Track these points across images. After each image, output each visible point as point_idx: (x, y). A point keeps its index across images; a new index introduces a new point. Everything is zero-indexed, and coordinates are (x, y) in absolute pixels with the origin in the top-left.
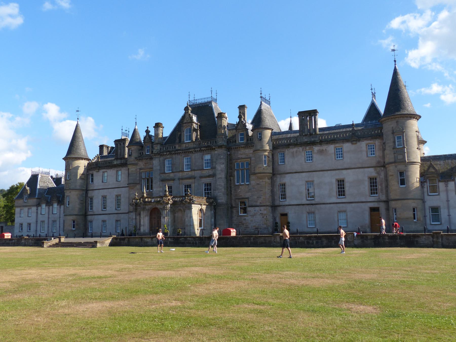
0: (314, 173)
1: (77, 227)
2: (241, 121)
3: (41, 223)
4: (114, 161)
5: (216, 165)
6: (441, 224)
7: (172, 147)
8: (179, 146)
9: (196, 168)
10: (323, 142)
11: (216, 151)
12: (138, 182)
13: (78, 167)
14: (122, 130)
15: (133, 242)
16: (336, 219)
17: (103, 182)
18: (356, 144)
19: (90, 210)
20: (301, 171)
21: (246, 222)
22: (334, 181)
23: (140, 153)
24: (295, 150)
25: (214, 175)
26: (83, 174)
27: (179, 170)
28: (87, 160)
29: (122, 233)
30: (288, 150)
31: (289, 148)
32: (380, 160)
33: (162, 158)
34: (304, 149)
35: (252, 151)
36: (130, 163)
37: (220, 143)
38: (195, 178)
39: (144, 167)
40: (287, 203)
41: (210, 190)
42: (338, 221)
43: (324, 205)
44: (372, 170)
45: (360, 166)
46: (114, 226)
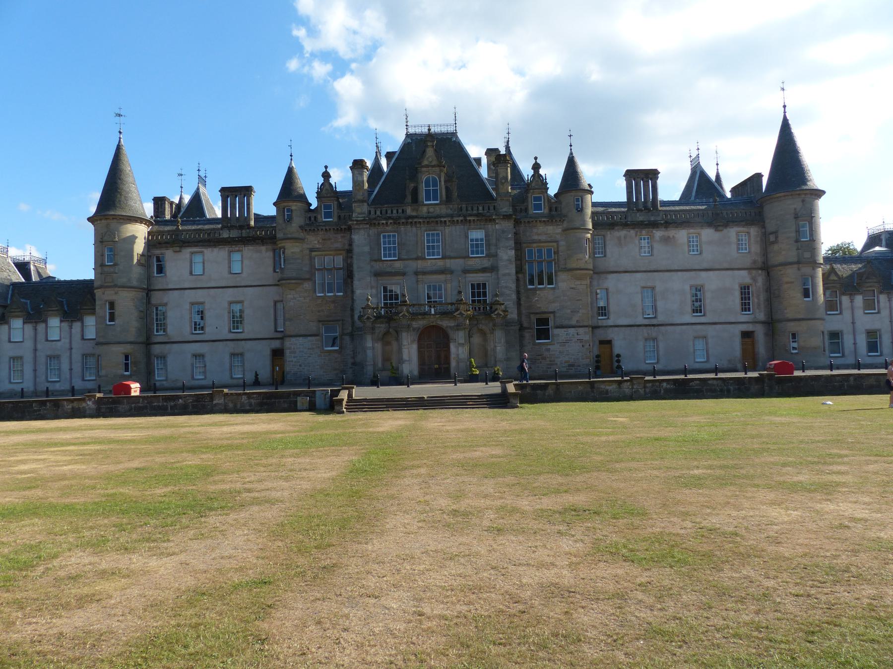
0: (224, 285)
1: (135, 369)
2: (537, 175)
3: (47, 360)
4: (221, 232)
5: (499, 251)
6: (843, 356)
7: (397, 210)
8: (413, 210)
9: (452, 254)
10: (670, 223)
11: (497, 224)
12: (307, 276)
13: (133, 238)
14: (199, 170)
15: (570, 392)
16: (691, 350)
17: (191, 273)
18: (722, 230)
19: (155, 333)
20: (634, 270)
21: (550, 355)
22: (687, 288)
23: (310, 217)
24: (623, 233)
25: (493, 269)
26: (142, 255)
27: (414, 256)
28: (145, 224)
29: (255, 380)
30: (611, 234)
31: (613, 229)
32: (756, 259)
33: (373, 231)
34: (638, 233)
35: (560, 230)
36: (289, 236)
37: (504, 210)
38: (451, 272)
39: (320, 246)
40: (610, 322)
41: (485, 295)
42: (694, 353)
43: (672, 327)
44: (744, 273)
45: (726, 266)
46: (227, 366)
